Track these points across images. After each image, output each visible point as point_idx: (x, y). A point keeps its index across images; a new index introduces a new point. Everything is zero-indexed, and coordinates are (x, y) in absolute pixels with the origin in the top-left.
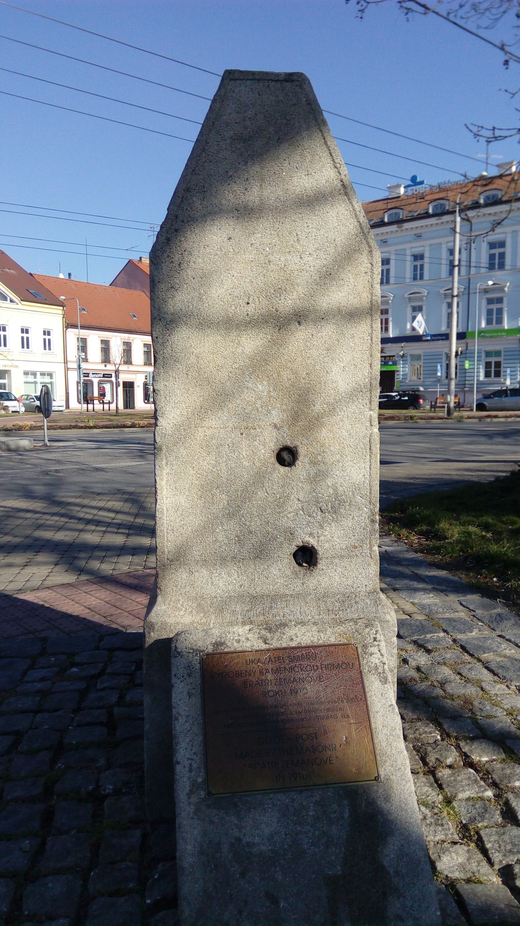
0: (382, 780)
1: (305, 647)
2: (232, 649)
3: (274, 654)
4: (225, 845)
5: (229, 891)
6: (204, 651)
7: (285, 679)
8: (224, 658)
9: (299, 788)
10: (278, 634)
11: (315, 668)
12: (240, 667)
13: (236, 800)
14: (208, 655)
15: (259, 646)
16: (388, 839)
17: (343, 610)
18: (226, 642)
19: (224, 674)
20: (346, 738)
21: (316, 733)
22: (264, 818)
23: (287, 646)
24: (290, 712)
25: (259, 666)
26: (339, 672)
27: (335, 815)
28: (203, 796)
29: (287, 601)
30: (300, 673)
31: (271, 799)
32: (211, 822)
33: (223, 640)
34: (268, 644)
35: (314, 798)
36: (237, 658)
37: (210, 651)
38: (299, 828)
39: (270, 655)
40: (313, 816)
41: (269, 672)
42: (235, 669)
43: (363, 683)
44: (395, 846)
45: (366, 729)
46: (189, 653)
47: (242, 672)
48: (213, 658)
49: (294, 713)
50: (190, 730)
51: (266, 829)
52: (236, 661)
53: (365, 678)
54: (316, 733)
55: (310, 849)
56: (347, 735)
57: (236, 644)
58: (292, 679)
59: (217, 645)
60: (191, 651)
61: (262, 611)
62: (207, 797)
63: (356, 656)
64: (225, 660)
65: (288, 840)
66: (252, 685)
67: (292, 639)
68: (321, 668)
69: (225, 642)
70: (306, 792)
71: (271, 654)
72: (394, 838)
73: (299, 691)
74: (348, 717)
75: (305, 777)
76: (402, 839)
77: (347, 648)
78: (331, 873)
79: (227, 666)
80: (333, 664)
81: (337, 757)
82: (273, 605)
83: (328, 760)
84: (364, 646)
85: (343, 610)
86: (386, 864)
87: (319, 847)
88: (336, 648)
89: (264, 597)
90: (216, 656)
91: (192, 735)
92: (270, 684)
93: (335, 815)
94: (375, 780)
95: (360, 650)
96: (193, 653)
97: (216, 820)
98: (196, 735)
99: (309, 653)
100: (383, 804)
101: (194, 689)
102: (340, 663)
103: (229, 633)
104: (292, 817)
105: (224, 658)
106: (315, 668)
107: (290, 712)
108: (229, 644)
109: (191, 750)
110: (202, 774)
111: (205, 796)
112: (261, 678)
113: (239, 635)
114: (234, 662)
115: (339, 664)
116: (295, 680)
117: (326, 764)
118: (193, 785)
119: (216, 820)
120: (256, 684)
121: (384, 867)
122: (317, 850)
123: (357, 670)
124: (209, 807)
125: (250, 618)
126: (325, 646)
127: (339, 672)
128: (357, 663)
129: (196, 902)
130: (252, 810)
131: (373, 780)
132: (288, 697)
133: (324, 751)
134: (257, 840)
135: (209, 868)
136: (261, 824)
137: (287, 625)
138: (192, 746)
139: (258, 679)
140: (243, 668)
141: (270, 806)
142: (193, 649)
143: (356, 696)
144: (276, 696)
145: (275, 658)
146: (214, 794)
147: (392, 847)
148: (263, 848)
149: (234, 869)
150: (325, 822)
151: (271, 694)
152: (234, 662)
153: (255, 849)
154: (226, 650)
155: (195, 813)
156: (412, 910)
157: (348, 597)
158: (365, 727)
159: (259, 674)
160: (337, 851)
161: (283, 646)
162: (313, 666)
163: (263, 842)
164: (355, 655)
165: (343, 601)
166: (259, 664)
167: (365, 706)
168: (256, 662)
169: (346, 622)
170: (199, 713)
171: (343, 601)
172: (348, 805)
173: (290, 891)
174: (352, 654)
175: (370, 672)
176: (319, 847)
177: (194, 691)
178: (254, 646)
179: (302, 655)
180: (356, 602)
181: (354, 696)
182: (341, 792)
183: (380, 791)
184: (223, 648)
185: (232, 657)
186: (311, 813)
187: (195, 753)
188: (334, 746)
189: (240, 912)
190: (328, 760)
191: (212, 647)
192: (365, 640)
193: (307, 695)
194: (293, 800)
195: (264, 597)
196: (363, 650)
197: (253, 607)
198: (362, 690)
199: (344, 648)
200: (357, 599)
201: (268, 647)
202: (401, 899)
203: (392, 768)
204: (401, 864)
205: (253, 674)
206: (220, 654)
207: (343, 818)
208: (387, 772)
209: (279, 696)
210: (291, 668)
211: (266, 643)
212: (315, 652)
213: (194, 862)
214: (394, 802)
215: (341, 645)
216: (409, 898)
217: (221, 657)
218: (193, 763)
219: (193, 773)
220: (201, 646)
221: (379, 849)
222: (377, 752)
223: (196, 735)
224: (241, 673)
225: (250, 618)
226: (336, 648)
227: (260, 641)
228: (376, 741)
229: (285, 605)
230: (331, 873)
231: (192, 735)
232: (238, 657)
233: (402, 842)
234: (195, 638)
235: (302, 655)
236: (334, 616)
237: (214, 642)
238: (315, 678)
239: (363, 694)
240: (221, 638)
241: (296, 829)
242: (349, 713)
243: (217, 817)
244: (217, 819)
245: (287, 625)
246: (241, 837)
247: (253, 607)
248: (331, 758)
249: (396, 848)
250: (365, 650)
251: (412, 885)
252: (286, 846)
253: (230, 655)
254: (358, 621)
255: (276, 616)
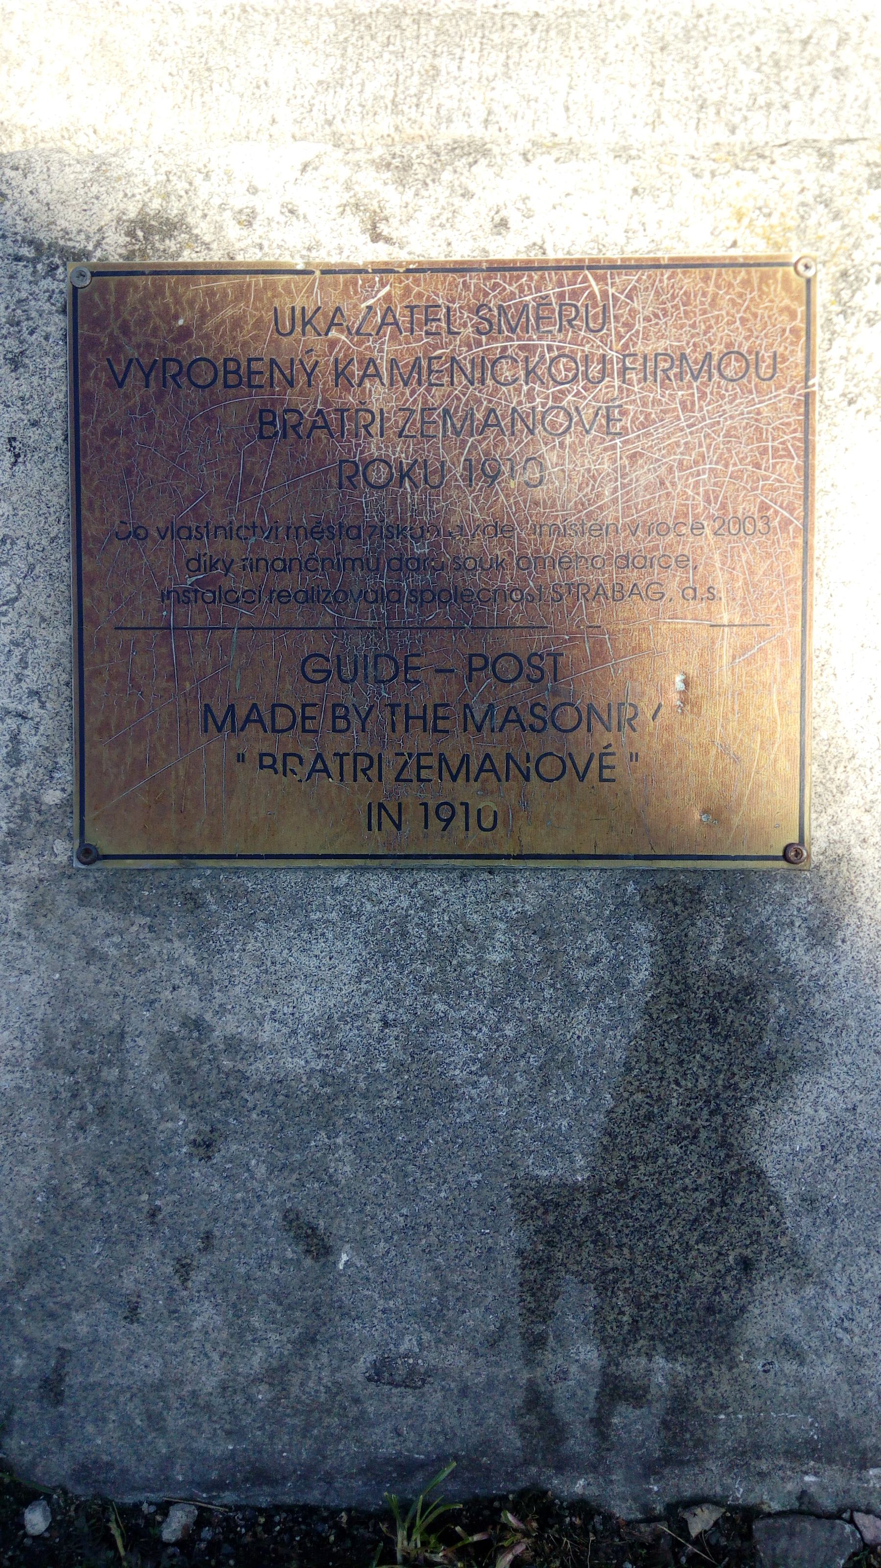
0: (815, 859)
1: (559, 267)
2: (216, 256)
3: (407, 290)
4: (141, 1042)
5: (145, 1197)
6: (87, 255)
7: (446, 411)
8: (174, 294)
9: (458, 863)
10: (439, 192)
11: (595, 370)
12: (245, 344)
13: (196, 883)
14: (101, 273)
15: (341, 251)
16: (797, 1078)
17: (769, 105)
18: (191, 220)
19: (173, 368)
20: (686, 682)
21: (556, 656)
22: (304, 959)
23: (477, 256)
24: (455, 559)
25: (333, 344)
26: (703, 396)
27: (592, 972)
28: (63, 859)
29: (511, 44)
30: (518, 391)
31: (337, 890)
32: (92, 955)
33: (173, 212)
34: (388, 240)
35: (517, 902)
36: (237, 300)
37: (114, 259)
38: (440, 1007)
39: (388, 298)
40: (504, 967)
41: (378, 375)
42: (221, 348)
43: (807, 449)
44: (821, 1110)
45: (784, 652)
46: (18, 259)
47: (255, 366)
48: (121, 294)
49: (470, 564)
50: (16, 599)
51: (307, 998)
52: (229, 312)
53: (820, 426)
54: (556, 656)
55: (474, 1085)
56: (692, 671)
57: (233, 232)
58: (479, 416)
59: (149, 231)
60: (26, 251)
61: (389, 95)
62: (76, 864)
63: (801, 325)
64: (177, 302)
65: (391, 1041)
66: (294, 427)
67: (503, 224)
68: (624, 370)
69: (183, 215)
70: (485, 876)
71: (398, 292)
72: (821, 1080)
73: (506, 469)
74: (711, 596)
75: (487, 823)
76: (854, 1086)
77: (763, 279)
78: (545, 1173)
79: (185, 333)
80: (683, 357)
81: (633, 757)
82: (442, 62)
83: (595, 764)
84: (844, 274)
85: (769, 105)
86: (768, 1165)
87: (510, 1081)
88: (706, 279)
89: (406, 21)
90: (140, 281)
91: (24, 620)
92: (375, 429)
93: (592, 972)
94: (785, 857)
95: (822, 295)
96: (34, 261)
97: (113, 952)
98: (43, 619)
99: (575, 294)
100: (801, 951)
101: (35, 424)
102: (717, 350)
103: (207, 176)
104: (417, 965)
105: (174, 294)
106: (595, 370)
107: (455, 559)
108: (203, 229)
109: (19, 678)
110: (66, 775)
111: (70, 859)
112: (338, 403)
113: (253, 190)
114: (217, 319)
115: (709, 356)
116: (491, 420)
117: (582, 778)
118: (24, 815)
119: (113, 952)
120: (314, 426)
121: (760, 1175)
122: (501, 1090)
123: (792, 391)
124: (83, 899)
125: (330, 123)
126: (656, 265)
127: (703, 396)
128: (800, 355)
129: (19, 1223)
130: (260, 924)
131: (775, 858)
132: (454, 493)
133: (584, 725)
134: (267, 1033)
135: (76, 1114)
136: (289, 978)
137: (486, 153)
138: (23, 663)
139: (326, 403)
140: (262, 349)
141: (334, 916)
142: (36, 244)
143: (764, 507)
144: (401, 484)
145: (411, 308)
146: (106, 857)
147: (809, 1110)
148: (293, 1064)
149: (170, 1125)
150: (547, 994)
151: (379, 474)
152: (217, 319)
153: (260, 1065)
154: (187, 257)
155: (29, 917)
156: (846, 1330)
157: (805, 43)
158: (782, 643)
159: (331, 379)
160: (582, 1101)
161: (457, 257)
162: (586, 359)
163: (292, 1041)
164: (793, 315)
165: (777, 64)
166: (333, 333)
167: (798, 554)
168: (322, 326)
169: (777, 151)
170: (54, 532)
171: (777, 64)
172: (652, 943)
173: (381, 1217)
174: (781, 311)
175: (851, 402)
176: (510, 1081)
177: (34, 434)
178: (318, 244)
179: (543, 303)
180: (839, 73)
181: (754, 510)
182: (631, 888)
183: (795, 901)
184: (171, 245)
185: (210, 293)
186: (495, 957)
187: (34, 693)
188: (629, 713)
189: (184, 1269)
190: (595, 764)
191: (124, 239)
192: (856, 246)
193: (539, 493)
194: (431, 903)
195: (406, 21)
196: (838, 294)
197: (351, 67)
198: (797, 484)
199: (746, 283)
200: (847, 57)
201: (384, 258)
202: (810, 1291)
203: (867, 819)
204: (831, 1175)
205: (302, 379)
206: (158, 272)
207: (624, 984)
208: (841, 831)
209: (415, 485)
210: (480, 364)
211: (376, 237)
212: (605, 294)
213: (19, 1088)
214: (846, 947)
215: (733, 264)
216: (841, 1290)
217: (159, 291)
218: (25, 729)
219: (23, 771)
220: (74, 228)
221: (754, 1112)
222: (814, 748)
223: (43, 619)
224: (250, 373)
225: (330, 123)
226: (706, 279)
227: (353, 223)
228: (817, 702)
229: (500, 69)
230: (545, 1173)
231: (24, 620)
232: (242, 293)
233: (855, 1097)
234: (43, 187)
235: (543, 303)
236: (721, 134)
237: (132, 214)
238: (587, 415)
239: (799, 503)
240: (167, 196)
241: (426, 1006)
242: (720, 580)
243: (116, 939)
244: (117, 946)
245: (486, 153)
246: (208, 1017)
247: (351, 67)
248: (608, 760)
249: (823, 1115)
250: (845, 295)
251: (861, 1249)
252: (381, 1066)
253: (202, 283)
254: (838, 150)
255: (449, 120)
